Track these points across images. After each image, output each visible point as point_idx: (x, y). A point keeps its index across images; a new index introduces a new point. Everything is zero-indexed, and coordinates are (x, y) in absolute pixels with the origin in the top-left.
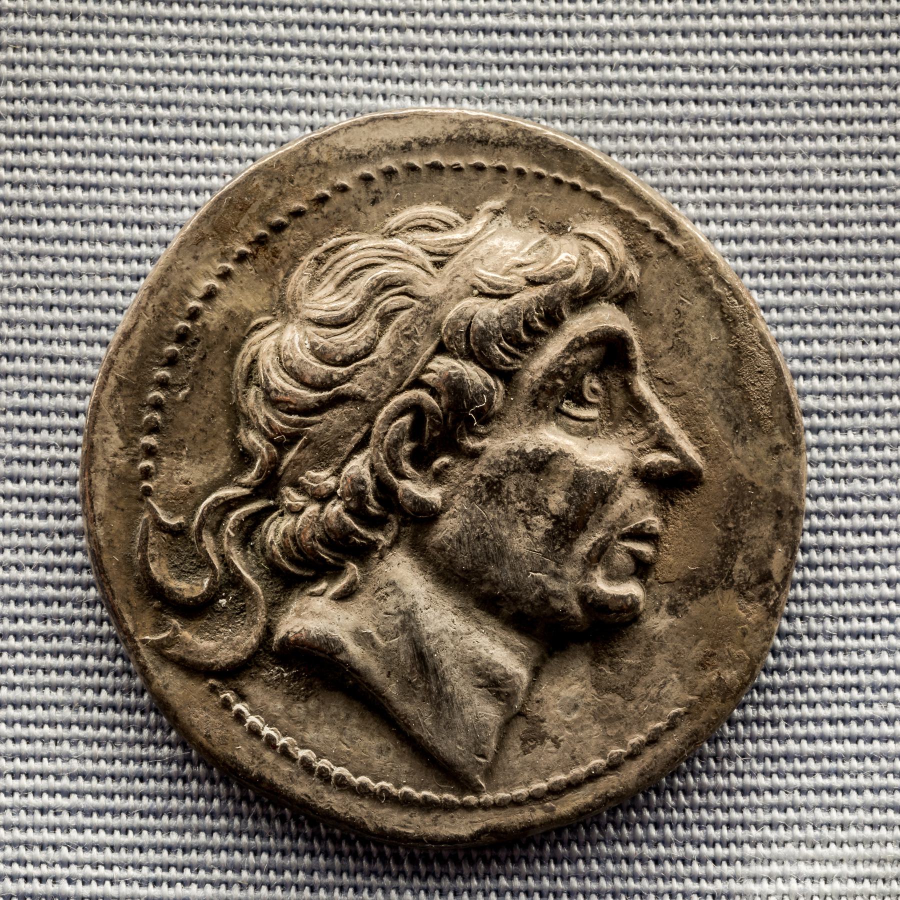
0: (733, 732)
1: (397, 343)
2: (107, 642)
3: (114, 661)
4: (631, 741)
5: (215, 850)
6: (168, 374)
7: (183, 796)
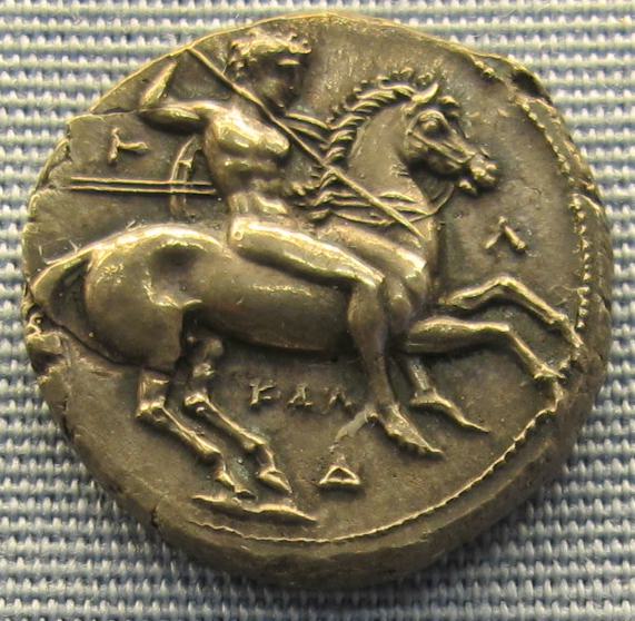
0: (590, 470)
1: (292, 199)
2: (61, 464)
3: (54, 445)
4: (516, 440)
5: (33, 479)
6: (148, 288)
7: (66, 517)
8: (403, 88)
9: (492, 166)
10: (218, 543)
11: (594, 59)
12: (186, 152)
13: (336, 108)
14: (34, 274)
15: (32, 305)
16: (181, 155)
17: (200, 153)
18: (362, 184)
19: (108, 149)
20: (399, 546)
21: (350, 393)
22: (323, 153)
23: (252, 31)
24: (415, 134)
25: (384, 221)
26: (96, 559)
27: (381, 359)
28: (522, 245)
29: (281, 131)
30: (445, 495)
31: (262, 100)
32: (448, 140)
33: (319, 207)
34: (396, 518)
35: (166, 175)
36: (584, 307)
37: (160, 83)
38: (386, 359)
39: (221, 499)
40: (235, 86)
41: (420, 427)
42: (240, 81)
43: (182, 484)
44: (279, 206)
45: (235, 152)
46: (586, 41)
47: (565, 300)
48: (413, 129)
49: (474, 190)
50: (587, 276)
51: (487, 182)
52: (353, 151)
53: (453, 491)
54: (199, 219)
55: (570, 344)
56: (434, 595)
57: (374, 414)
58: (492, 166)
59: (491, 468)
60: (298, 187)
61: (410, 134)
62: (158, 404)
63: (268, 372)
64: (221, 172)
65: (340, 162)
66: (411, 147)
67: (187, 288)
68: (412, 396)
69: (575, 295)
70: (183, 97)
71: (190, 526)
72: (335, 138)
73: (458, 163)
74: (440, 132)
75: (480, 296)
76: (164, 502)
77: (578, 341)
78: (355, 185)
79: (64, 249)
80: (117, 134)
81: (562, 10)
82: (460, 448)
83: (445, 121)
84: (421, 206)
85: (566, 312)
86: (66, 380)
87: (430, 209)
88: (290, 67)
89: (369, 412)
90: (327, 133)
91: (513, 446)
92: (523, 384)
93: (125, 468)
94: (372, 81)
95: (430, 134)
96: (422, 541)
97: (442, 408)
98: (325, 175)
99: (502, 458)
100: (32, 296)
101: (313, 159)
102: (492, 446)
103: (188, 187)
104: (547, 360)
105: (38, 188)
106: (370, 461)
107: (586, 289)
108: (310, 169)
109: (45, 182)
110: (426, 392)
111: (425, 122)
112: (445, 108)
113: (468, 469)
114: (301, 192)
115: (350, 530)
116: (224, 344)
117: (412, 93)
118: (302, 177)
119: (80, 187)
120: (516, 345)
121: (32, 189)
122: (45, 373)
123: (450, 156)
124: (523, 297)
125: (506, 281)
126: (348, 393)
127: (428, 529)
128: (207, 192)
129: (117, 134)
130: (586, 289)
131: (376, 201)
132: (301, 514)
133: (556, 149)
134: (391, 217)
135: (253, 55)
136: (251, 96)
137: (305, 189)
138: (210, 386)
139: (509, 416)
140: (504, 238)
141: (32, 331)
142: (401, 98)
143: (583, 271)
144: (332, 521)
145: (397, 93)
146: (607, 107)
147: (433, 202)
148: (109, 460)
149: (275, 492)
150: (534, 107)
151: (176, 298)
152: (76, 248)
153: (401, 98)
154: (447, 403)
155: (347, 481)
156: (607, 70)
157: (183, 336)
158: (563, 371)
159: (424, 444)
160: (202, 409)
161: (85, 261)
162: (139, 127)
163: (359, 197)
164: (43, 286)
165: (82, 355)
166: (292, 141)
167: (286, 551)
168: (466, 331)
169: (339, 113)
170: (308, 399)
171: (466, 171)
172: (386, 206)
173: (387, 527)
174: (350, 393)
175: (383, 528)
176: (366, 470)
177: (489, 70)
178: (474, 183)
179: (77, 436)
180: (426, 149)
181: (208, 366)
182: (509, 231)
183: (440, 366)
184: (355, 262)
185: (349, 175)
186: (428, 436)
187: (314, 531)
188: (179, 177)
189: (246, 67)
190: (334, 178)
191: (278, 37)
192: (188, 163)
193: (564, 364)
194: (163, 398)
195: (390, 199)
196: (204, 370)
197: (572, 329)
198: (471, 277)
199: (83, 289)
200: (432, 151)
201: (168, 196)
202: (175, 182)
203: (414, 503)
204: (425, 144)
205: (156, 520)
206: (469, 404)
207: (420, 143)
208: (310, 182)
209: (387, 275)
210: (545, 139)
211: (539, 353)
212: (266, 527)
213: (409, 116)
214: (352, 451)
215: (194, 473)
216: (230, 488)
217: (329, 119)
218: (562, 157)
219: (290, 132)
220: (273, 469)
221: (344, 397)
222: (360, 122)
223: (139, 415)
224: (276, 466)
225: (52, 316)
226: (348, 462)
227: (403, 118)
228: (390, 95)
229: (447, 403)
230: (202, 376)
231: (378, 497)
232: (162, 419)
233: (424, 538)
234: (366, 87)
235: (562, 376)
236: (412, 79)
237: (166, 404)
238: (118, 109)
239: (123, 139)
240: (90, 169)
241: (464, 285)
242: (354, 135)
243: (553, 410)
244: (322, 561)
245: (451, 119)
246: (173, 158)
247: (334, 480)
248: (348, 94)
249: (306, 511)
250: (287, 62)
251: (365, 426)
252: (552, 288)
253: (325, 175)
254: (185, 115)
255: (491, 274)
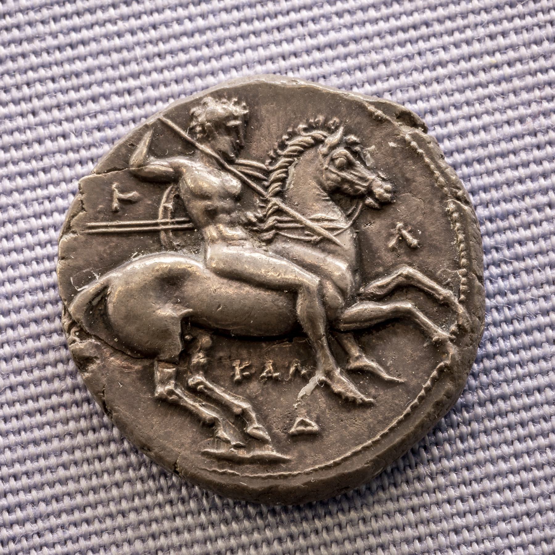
1: (248, 225)
8: (318, 133)
9: (388, 186)
10: (223, 482)
11: (480, 91)
12: (168, 197)
13: (271, 153)
14: (70, 300)
15: (71, 321)
16: (164, 199)
17: (178, 197)
18: (297, 210)
19: (111, 201)
20: (350, 471)
21: (303, 365)
22: (266, 188)
23: (205, 100)
24: (330, 168)
25: (315, 238)
26: (142, 495)
27: (324, 338)
28: (415, 242)
29: (235, 175)
30: (379, 431)
31: (219, 155)
32: (355, 170)
33: (267, 230)
34: (346, 451)
35: (155, 217)
36: (463, 284)
37: (142, 148)
38: (327, 338)
39: (222, 451)
40: (198, 144)
41: (356, 383)
42: (201, 141)
43: (194, 442)
44: (239, 232)
45: (204, 196)
46: (472, 79)
47: (449, 280)
48: (329, 164)
49: (377, 205)
50: (464, 261)
51: (386, 199)
52: (287, 185)
53: (384, 428)
54: (183, 247)
55: (455, 312)
56: (376, 498)
57: (323, 378)
58: (388, 186)
59: (409, 409)
60: (250, 215)
61: (327, 169)
62: (170, 386)
63: (244, 353)
64: (194, 211)
65: (278, 194)
66: (328, 179)
67: (183, 302)
68: (348, 362)
69: (456, 276)
70: (161, 155)
71: (202, 472)
72: (273, 176)
73: (364, 187)
74: (349, 165)
75: (388, 284)
76: (182, 456)
77: (461, 309)
78: (292, 212)
79: (89, 279)
80: (116, 188)
81: (448, 60)
82: (385, 395)
83: (351, 157)
84: (344, 224)
85: (451, 288)
86: (103, 375)
87: (346, 223)
88: (236, 127)
89: (319, 376)
90: (267, 173)
91: (423, 391)
92: (425, 345)
93: (151, 434)
94: (296, 130)
95: (341, 168)
96: (366, 466)
97: (370, 369)
98: (270, 205)
99: (416, 401)
100: (70, 315)
101: (260, 194)
102: (408, 392)
103: (173, 223)
104: (441, 325)
105: (64, 233)
106: (323, 412)
107: (464, 270)
108: (258, 201)
109: (68, 229)
110: (357, 358)
111: (337, 158)
112: (349, 146)
113: (394, 410)
114: (254, 220)
115: (315, 463)
116: (212, 338)
117: (325, 137)
118: (254, 208)
119: (94, 231)
120: (417, 317)
121: (59, 233)
122: (86, 371)
123: (357, 182)
124: (419, 282)
125: (407, 270)
126: (302, 365)
127: (371, 456)
128: (186, 226)
129: (116, 188)
130: (464, 270)
131: (309, 223)
132: (279, 455)
133: (432, 166)
134: (319, 234)
135: (208, 121)
136: (209, 151)
137: (256, 217)
138: (206, 369)
139: (418, 369)
140: (402, 240)
141: (74, 341)
142: (318, 142)
143: (460, 258)
144: (302, 457)
145: (314, 138)
146: (497, 125)
147: (349, 216)
148: (140, 430)
149: (261, 442)
150: (415, 137)
151: (174, 309)
152: (97, 277)
153: (318, 142)
154: (374, 365)
155: (309, 428)
156: (491, 98)
157: (182, 336)
158: (453, 333)
159: (360, 396)
160: (202, 386)
161: (105, 288)
162: (131, 182)
163: (296, 221)
164: (78, 308)
165: (111, 355)
166: (243, 182)
167: (272, 483)
168: (381, 311)
169: (274, 156)
170: (276, 370)
171: (370, 192)
172: (315, 225)
173: (340, 458)
174: (303, 365)
175: (337, 459)
176: (321, 419)
177: (379, 112)
178: (376, 200)
179: (114, 414)
180: (339, 179)
181: (201, 355)
182: (404, 232)
183: (365, 339)
184: (297, 269)
185: (286, 204)
186: (362, 389)
187: (290, 466)
188: (165, 217)
189: (203, 131)
190: (276, 207)
191: (224, 103)
192: (170, 206)
193: (453, 328)
194: (173, 382)
195: (318, 220)
196: (199, 358)
197: (456, 301)
198: (381, 269)
199: (106, 307)
200: (345, 180)
201: (157, 232)
202: (163, 221)
203: (358, 439)
204: (338, 175)
205: (178, 469)
206: (388, 364)
207: (334, 175)
208: (259, 211)
209: (322, 278)
210: (424, 162)
211: (435, 321)
212: (255, 467)
213: (325, 156)
214: (310, 406)
215: (201, 433)
216: (228, 442)
217: (268, 161)
218: (437, 173)
219: (241, 175)
220: (256, 425)
221: (300, 368)
222: (290, 163)
223: (156, 395)
224: (259, 421)
225: (87, 329)
226: (309, 413)
227: (321, 157)
228: (309, 139)
229: (374, 365)
230: (198, 362)
231: (331, 437)
232: (174, 397)
233: (367, 463)
234: (293, 135)
235: (453, 337)
236: (325, 127)
237: (176, 386)
238: (115, 169)
239: (122, 191)
240: (101, 216)
241: (377, 276)
242: (287, 173)
243: (448, 362)
244: (298, 487)
245: (355, 153)
246: (159, 202)
247: (301, 428)
248: (279, 140)
249: (283, 452)
250: (232, 123)
251: (317, 387)
252: (439, 272)
253: (270, 205)
254: (164, 169)
255: (395, 266)
